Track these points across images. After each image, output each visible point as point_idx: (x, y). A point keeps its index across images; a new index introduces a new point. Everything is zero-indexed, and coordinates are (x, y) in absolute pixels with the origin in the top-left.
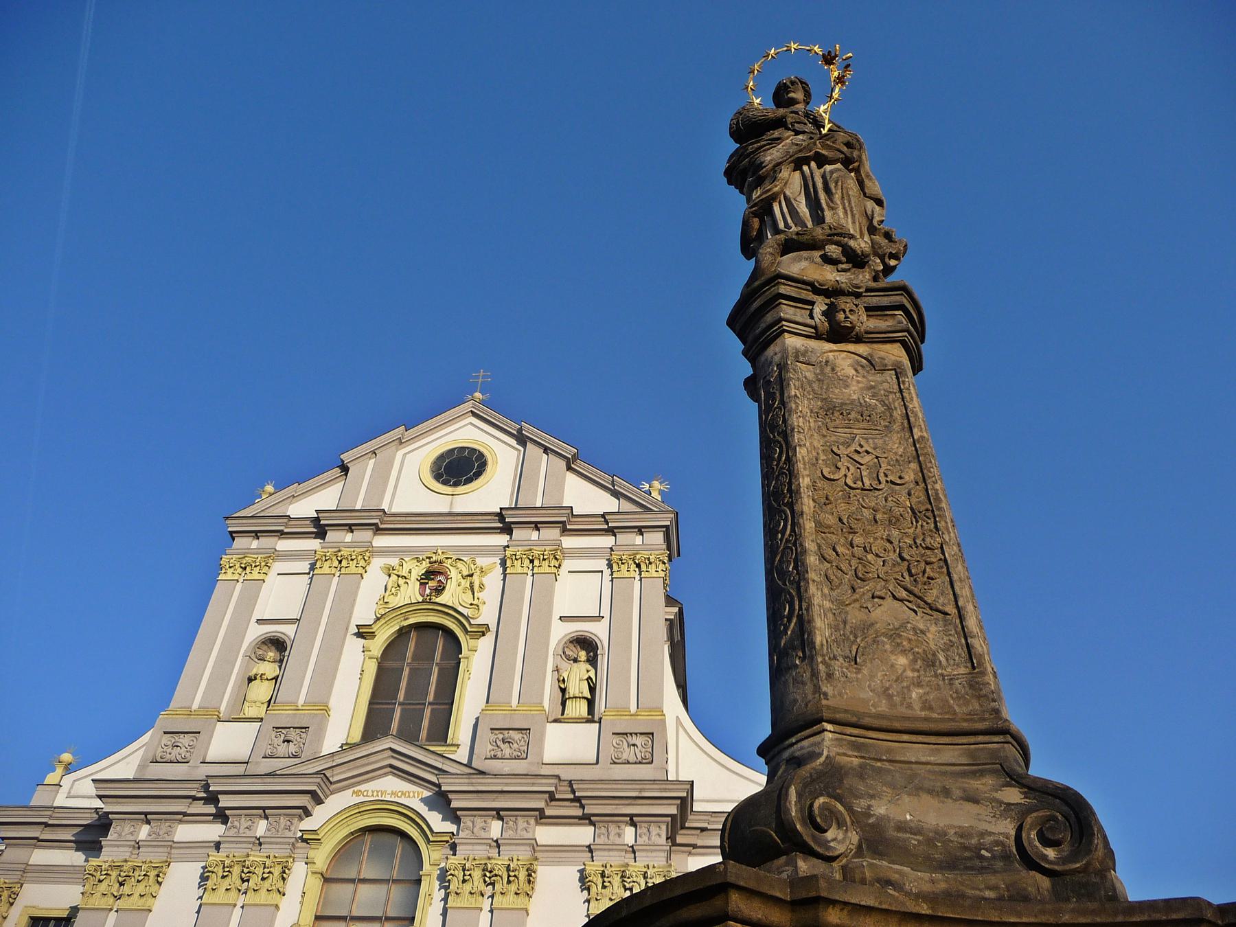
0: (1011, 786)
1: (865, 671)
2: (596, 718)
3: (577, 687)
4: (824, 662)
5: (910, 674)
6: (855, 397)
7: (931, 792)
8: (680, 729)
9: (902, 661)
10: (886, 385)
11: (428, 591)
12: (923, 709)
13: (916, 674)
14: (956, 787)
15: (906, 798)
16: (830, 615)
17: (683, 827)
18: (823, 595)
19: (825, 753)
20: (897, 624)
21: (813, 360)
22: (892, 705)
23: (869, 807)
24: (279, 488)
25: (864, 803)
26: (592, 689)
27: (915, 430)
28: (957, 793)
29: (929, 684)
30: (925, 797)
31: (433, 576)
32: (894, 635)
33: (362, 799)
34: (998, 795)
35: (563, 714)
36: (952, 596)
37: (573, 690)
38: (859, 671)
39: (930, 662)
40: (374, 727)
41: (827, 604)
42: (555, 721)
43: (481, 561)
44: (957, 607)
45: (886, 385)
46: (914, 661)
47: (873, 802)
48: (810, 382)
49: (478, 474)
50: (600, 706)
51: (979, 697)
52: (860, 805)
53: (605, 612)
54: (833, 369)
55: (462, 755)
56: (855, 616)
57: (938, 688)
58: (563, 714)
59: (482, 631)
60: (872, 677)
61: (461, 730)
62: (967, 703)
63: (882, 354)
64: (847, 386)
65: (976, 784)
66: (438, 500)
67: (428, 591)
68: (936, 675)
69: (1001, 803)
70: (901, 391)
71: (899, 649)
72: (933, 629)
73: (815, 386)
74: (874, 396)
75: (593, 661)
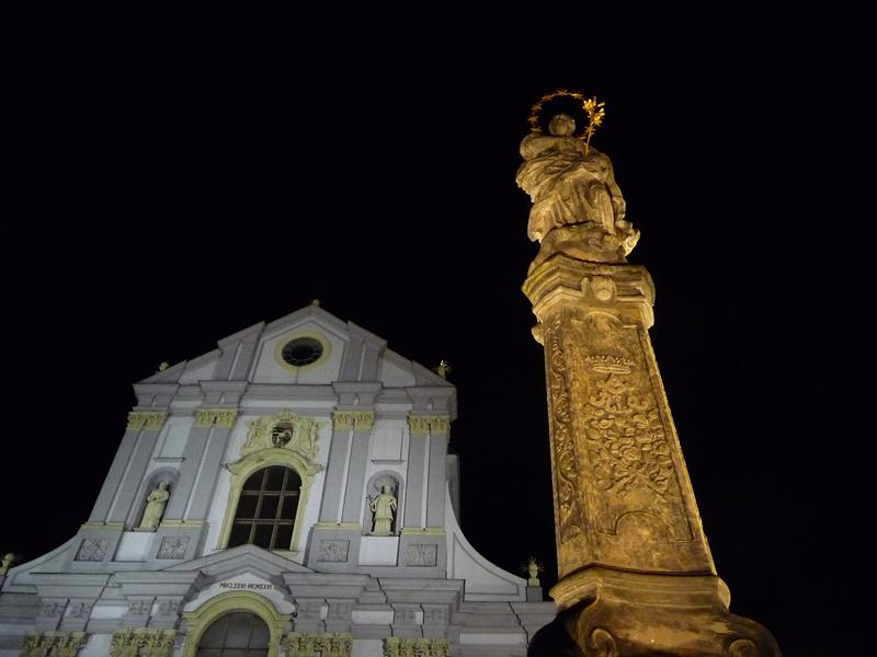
0: (720, 621)
1: (622, 540)
2: (397, 533)
3: (384, 512)
4: (595, 533)
5: (651, 542)
6: (610, 345)
7: (667, 625)
8: (457, 544)
9: (645, 533)
10: (630, 338)
11: (278, 440)
12: (661, 566)
13: (655, 542)
14: (683, 621)
15: (651, 629)
16: (598, 500)
17: (451, 605)
18: (593, 486)
19: (598, 597)
20: (641, 507)
21: (655, 403)
22: (639, 563)
23: (627, 635)
24: (171, 365)
25: (624, 632)
26: (394, 514)
27: (651, 370)
28: (685, 626)
29: (664, 549)
30: (664, 628)
31: (282, 434)
32: (640, 513)
33: (227, 589)
34: (712, 628)
35: (373, 530)
36: (677, 488)
37: (379, 514)
38: (618, 539)
39: (664, 534)
40: (237, 537)
41: (595, 492)
42: (368, 535)
43: (317, 419)
44: (681, 496)
45: (630, 338)
46: (653, 533)
47: (631, 632)
48: (580, 335)
49: (316, 358)
50: (400, 524)
51: (697, 559)
52: (621, 634)
53: (405, 457)
54: (595, 325)
55: (300, 558)
56: (614, 502)
57: (670, 552)
58: (373, 530)
59: (319, 468)
60: (626, 544)
61: (300, 539)
62: (689, 562)
63: (627, 315)
64: (604, 338)
65: (696, 619)
66: (287, 373)
67: (278, 440)
68: (668, 543)
69: (712, 632)
70: (641, 342)
71: (643, 524)
72: (666, 510)
73: (584, 338)
74: (622, 345)
75: (395, 494)
